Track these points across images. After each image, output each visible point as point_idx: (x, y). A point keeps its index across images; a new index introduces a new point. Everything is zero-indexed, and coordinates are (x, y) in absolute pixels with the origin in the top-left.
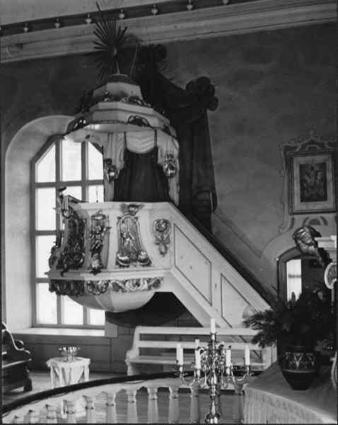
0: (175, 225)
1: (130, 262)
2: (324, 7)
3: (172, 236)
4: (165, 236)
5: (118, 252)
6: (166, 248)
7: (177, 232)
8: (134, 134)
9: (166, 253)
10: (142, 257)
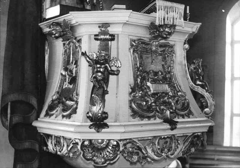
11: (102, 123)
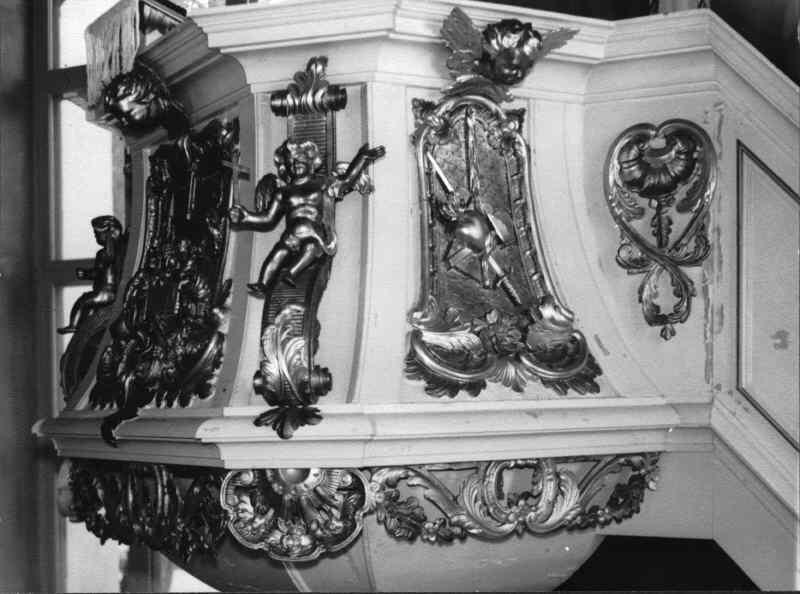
0: (742, 149)
1: (482, 365)
2: (166, 507)
3: (720, 217)
4: (680, 221)
5: (420, 306)
6: (683, 290)
7: (759, 189)
8: (163, 584)
9: (680, 315)
10: (546, 337)
11: (165, 395)
